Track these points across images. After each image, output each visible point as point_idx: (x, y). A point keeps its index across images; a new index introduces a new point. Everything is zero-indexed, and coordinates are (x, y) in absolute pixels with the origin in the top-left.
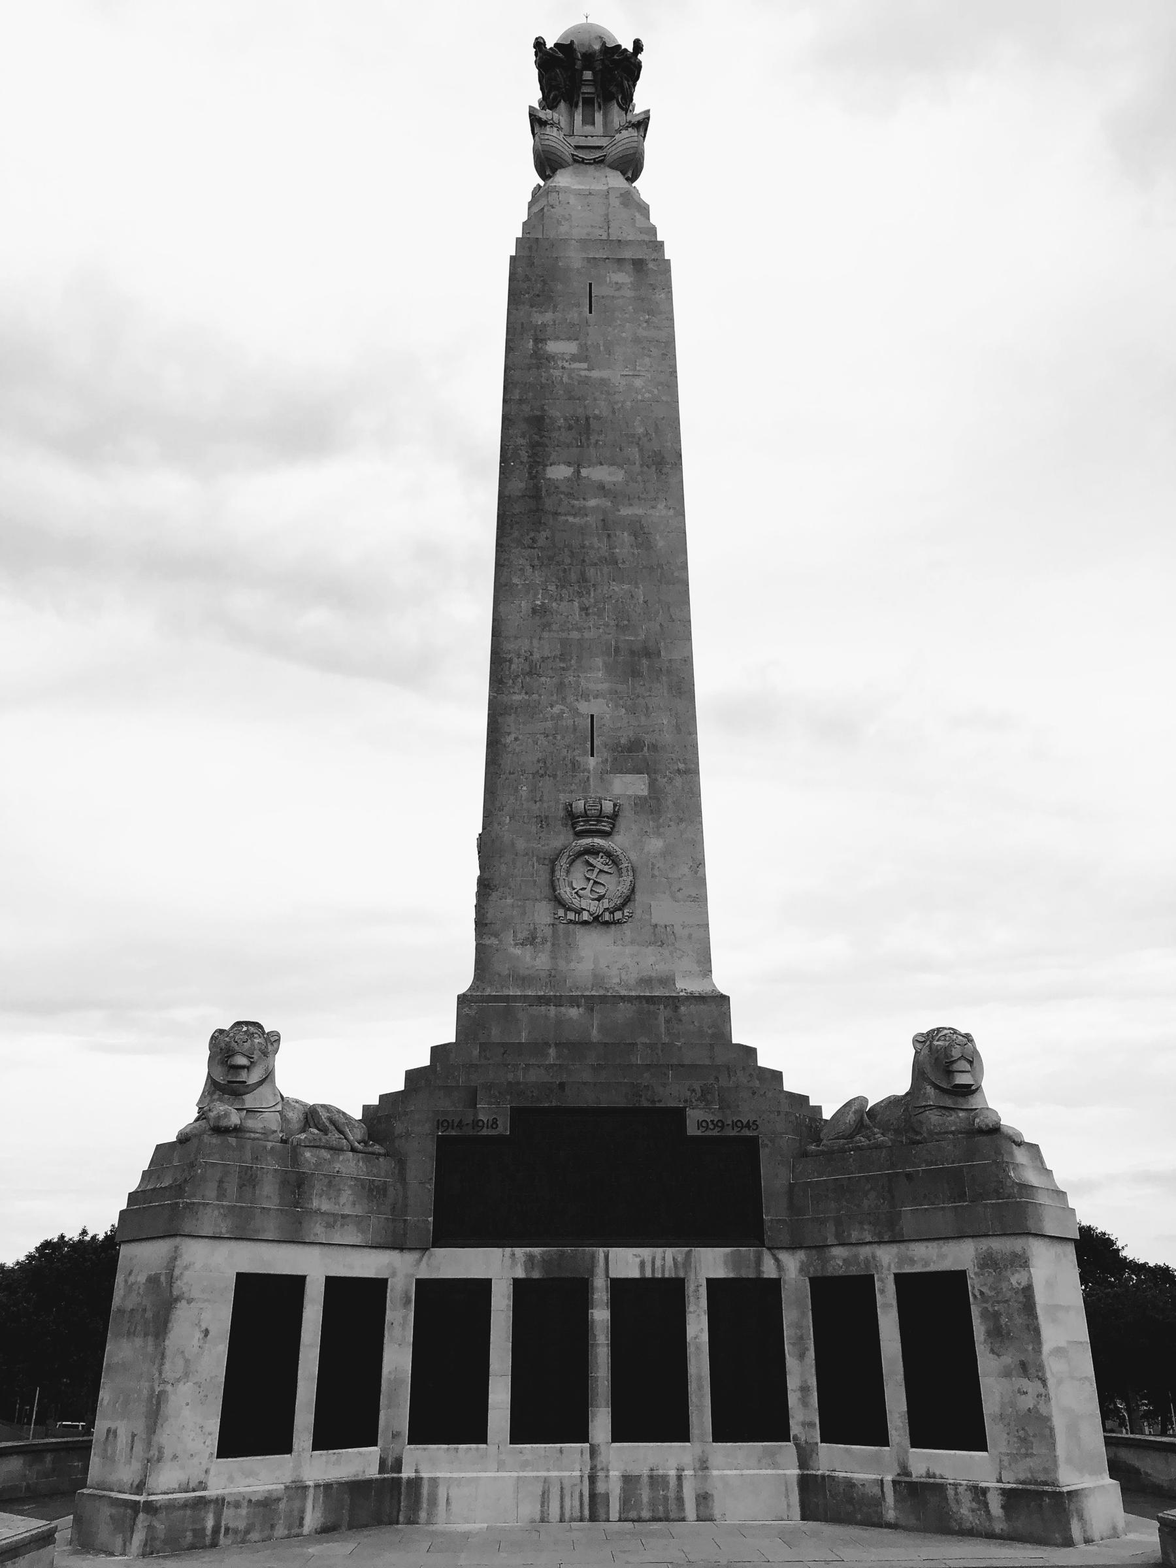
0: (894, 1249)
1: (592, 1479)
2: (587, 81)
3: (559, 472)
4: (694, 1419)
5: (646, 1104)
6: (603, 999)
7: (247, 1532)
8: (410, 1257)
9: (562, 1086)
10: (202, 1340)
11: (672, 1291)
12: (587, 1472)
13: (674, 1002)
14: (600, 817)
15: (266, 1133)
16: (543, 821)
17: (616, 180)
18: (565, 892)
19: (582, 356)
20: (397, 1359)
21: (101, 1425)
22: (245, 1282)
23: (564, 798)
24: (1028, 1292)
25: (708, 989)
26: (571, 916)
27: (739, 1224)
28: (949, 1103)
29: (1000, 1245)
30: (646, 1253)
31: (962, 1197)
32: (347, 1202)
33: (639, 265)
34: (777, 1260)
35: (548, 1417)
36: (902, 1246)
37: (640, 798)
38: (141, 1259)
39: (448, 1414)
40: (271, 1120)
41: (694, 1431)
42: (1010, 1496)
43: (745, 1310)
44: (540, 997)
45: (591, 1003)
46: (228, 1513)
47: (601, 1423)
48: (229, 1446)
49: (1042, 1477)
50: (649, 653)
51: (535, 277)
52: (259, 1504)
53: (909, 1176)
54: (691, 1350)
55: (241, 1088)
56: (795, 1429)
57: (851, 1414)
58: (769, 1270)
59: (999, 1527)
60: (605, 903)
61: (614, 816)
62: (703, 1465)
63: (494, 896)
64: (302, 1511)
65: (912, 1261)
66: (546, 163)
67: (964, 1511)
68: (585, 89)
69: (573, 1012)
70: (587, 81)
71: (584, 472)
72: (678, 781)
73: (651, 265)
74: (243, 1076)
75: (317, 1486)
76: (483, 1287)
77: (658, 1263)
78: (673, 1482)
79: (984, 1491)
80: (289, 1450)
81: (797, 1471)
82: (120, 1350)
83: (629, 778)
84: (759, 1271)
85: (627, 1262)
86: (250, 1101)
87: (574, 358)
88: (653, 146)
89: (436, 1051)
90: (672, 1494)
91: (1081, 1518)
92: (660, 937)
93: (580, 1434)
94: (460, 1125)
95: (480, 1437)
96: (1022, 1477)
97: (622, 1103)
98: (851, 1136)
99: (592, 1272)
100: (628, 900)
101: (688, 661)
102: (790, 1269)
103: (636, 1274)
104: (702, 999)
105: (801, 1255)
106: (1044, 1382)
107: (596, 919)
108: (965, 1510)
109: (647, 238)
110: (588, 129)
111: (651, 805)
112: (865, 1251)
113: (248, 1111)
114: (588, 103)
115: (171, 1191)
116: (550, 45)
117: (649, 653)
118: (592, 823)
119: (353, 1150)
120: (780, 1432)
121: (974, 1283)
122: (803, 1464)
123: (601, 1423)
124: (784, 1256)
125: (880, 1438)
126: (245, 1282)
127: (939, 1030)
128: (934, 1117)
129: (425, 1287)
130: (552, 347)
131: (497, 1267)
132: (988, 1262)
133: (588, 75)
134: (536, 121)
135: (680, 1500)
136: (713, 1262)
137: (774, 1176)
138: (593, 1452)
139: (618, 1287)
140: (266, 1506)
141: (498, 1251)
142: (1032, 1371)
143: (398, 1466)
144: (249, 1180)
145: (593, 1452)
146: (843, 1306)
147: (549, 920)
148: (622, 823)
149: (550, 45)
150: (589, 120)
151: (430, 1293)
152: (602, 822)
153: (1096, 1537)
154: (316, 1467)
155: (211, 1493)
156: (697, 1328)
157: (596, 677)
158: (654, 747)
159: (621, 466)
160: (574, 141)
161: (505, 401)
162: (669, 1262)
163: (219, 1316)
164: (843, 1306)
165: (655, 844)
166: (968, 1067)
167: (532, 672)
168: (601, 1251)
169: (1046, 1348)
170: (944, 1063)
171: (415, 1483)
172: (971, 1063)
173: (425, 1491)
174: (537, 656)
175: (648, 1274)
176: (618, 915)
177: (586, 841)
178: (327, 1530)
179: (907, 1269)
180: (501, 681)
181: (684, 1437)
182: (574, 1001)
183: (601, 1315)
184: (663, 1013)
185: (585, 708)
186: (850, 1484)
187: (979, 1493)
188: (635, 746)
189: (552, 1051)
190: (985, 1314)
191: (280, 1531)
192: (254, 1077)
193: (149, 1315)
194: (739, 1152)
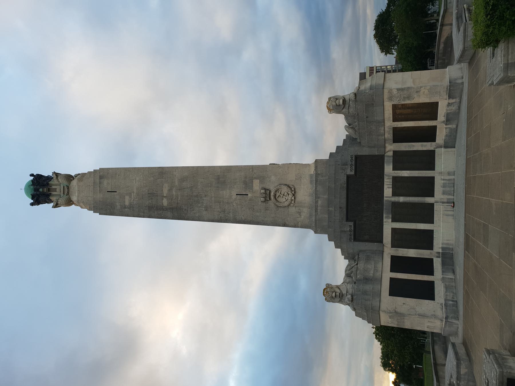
0: (386, 122)
1: (443, 203)
2: (42, 190)
3: (165, 202)
4: (429, 175)
5: (346, 185)
6: (316, 194)
7: (453, 293)
8: (385, 249)
9: (340, 208)
10: (406, 304)
11: (396, 180)
12: (441, 204)
13: (317, 175)
14: (265, 193)
15: (353, 288)
16: (266, 209)
17: (74, 183)
18: (286, 204)
19: (130, 195)
20: (412, 253)
21: (426, 329)
22: (391, 294)
23: (260, 203)
24: (398, 90)
25: (313, 165)
26: (293, 202)
27: (378, 161)
28: (347, 106)
29: (386, 96)
30: (385, 187)
31: (373, 104)
32: (371, 266)
33: (101, 177)
34: (388, 151)
35: (427, 213)
36: (385, 119)
37: (260, 182)
38: (385, 320)
39: (426, 239)
40: (349, 286)
41: (432, 175)
42: (450, 97)
43: (401, 160)
44: (315, 211)
45: (317, 197)
46: (448, 298)
47: (429, 200)
48: (431, 297)
49: (445, 89)
50: (218, 178)
51: (106, 208)
52: (446, 290)
53: (367, 117)
54: (411, 175)
55: (341, 294)
56: (432, 149)
57: (429, 134)
58: (391, 154)
59: (458, 100)
60: (289, 193)
61: (266, 189)
62: (441, 173)
63: (287, 223)
64: (449, 278)
65: (390, 117)
66: (69, 203)
67: (454, 108)
68: (45, 191)
69: (320, 202)
70: (42, 190)
71: (165, 195)
72: (255, 171)
73: (101, 174)
74: (338, 294)
75: (443, 274)
76: (394, 230)
77: (388, 183)
78: (445, 182)
79: (449, 103)
80: (433, 282)
81: (443, 149)
82: (408, 325)
83: (254, 185)
84: (391, 157)
85: (388, 191)
86: (344, 292)
87: (130, 197)
88: (63, 171)
89: (330, 240)
90: (448, 182)
91: (456, 79)
92: (299, 178)
93: (432, 205)
94: (351, 235)
95: (432, 231)
96: (445, 94)
97: (345, 192)
98: (356, 131)
99: (391, 201)
100: (289, 186)
101: (221, 167)
102: (391, 148)
103: (391, 189)
104: (316, 167)
105: (387, 145)
106: (421, 87)
107: (294, 195)
108: (454, 108)
109: (92, 175)
110: (57, 190)
111: (262, 179)
112: (386, 129)
113: (347, 292)
114: (49, 190)
115: (365, 308)
116: (32, 201)
117: (218, 178)
118: (267, 195)
119: (357, 264)
120: (433, 152)
121: (395, 102)
122: (441, 147)
123: (429, 200)
124: (387, 150)
125: (435, 127)
126: (391, 294)
127: (327, 107)
128: (351, 110)
129: (393, 246)
130: (127, 203)
131: (388, 226)
132: (390, 99)
133: (41, 190)
134: (56, 206)
135: (449, 180)
136: (388, 169)
137: (365, 151)
138: (437, 202)
139: (394, 194)
140: (447, 288)
141: (384, 226)
142: (418, 90)
143: (439, 253)
144: (365, 293)
145: (437, 202)
146: (399, 136)
147: (294, 208)
148: (267, 187)
149: (32, 201)
150: (55, 190)
151: (394, 245)
152: (267, 195)
153: (461, 75)
154: (438, 277)
155: (443, 302)
156: (405, 173)
157: (225, 193)
158: (246, 177)
159: (163, 185)
160: (62, 195)
161: (144, 217)
162: (388, 180)
163: (400, 300)
164: (399, 136)
165: (273, 178)
166: (338, 100)
167: (224, 211)
168: (385, 199)
169: (413, 86)
170: (337, 105)
171: (443, 248)
172: (337, 99)
173: (445, 246)
174: (219, 210)
175: (391, 186)
176: (293, 189)
177: (272, 197)
178: (454, 272)
179: (392, 119)
180: (227, 220)
181: (433, 178)
182: (316, 202)
183: (402, 199)
184: (320, 178)
185: (234, 196)
186: (446, 136)
187: (449, 105)
188: (245, 183)
189: (330, 209)
190: (404, 100)
191: (453, 284)
192: (338, 291)
193: (399, 318)
194: (359, 160)
